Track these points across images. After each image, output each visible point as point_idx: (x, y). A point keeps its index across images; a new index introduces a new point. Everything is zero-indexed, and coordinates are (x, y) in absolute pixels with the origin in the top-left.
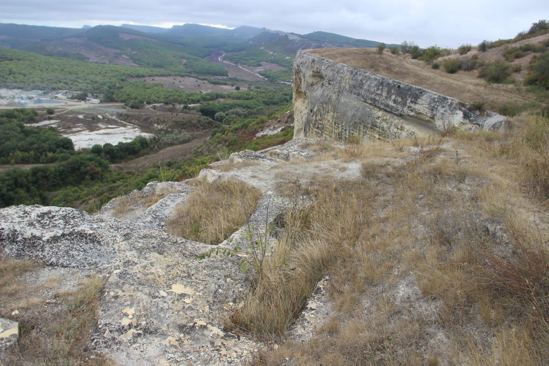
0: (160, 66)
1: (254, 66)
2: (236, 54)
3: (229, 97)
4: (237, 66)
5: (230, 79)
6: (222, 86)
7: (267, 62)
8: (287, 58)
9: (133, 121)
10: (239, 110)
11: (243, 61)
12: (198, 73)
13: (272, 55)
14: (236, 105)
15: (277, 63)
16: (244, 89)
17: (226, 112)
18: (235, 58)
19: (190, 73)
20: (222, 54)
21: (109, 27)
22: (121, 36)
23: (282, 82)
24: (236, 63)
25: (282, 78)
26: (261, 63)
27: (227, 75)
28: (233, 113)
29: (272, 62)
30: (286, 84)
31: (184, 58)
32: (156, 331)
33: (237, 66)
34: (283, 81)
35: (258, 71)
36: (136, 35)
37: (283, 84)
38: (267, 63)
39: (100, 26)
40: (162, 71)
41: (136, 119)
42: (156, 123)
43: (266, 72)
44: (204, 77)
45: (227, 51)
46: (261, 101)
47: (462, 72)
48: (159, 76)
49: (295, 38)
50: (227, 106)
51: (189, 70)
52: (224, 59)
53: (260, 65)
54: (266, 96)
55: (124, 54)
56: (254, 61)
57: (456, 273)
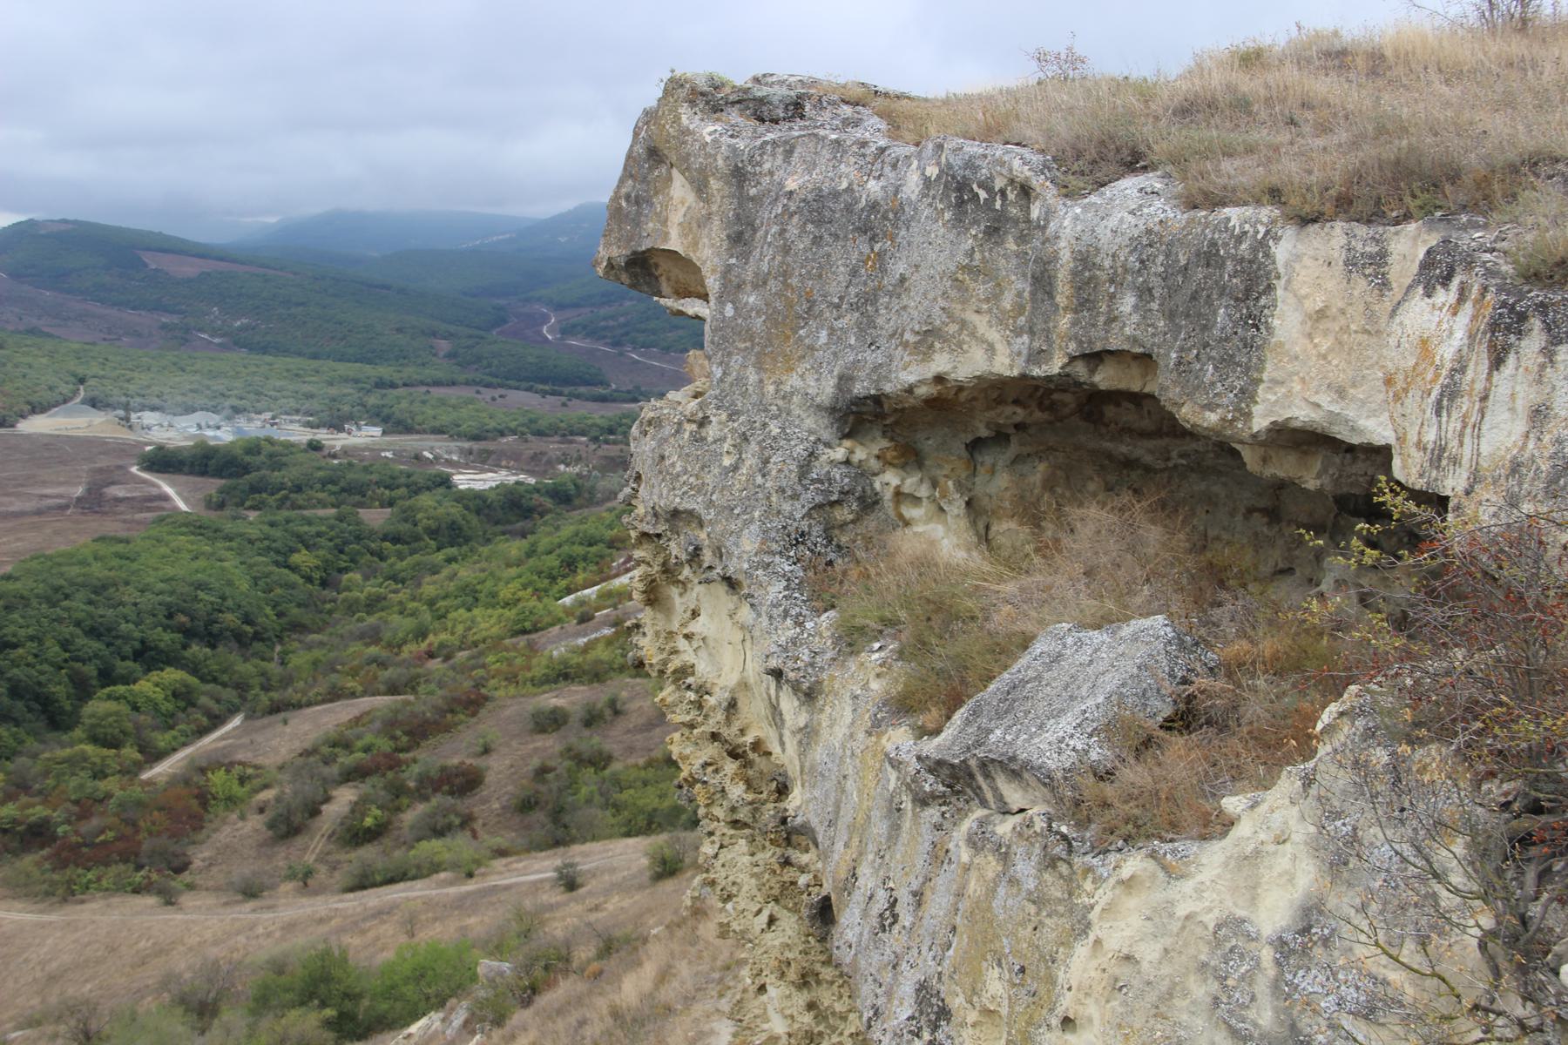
2: (604, 311)
9: (504, 463)
11: (641, 338)
18: (605, 328)
22: (147, 257)
24: (616, 344)
27: (606, 384)
32: (537, 803)
33: (621, 354)
40: (410, 372)
41: (510, 458)
42: (562, 462)
45: (560, 307)
47: (1472, 161)
55: (200, 330)
56: (681, 332)
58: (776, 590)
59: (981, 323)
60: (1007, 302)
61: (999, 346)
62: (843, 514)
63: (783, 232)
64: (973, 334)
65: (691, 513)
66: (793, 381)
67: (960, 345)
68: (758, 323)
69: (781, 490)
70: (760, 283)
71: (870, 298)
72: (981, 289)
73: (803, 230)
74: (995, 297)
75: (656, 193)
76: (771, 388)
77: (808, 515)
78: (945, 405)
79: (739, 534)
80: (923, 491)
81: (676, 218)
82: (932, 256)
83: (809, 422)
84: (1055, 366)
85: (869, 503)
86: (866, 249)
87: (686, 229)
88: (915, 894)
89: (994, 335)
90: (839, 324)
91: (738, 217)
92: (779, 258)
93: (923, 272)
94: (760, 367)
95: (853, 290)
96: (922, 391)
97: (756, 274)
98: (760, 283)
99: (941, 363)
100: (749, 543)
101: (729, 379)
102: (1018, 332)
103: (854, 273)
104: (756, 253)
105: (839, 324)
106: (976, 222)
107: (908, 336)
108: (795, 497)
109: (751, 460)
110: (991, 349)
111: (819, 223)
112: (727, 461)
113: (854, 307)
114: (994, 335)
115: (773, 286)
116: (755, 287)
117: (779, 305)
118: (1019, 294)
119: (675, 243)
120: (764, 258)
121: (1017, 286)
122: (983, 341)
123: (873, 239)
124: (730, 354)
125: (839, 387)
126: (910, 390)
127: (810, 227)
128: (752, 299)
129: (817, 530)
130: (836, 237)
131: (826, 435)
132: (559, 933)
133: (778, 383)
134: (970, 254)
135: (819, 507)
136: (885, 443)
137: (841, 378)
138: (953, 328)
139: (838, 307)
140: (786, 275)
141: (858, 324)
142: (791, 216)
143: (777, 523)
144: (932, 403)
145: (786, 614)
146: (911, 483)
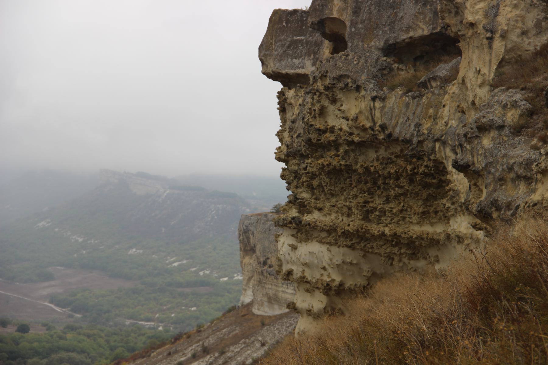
8: (133, 251)
34: (131, 318)
35: (45, 292)
58: (371, 86)
59: (421, 24)
60: (427, 19)
61: (425, 29)
62: (385, 72)
63: (369, 9)
64: (419, 27)
65: (346, 75)
66: (373, 43)
67: (416, 30)
68: (362, 31)
69: (371, 66)
70: (363, 22)
71: (393, 22)
72: (421, 17)
73: (375, 8)
74: (425, 18)
75: (329, 3)
76: (366, 46)
77: (378, 71)
78: (412, 43)
79: (361, 76)
80: (404, 68)
81: (335, 9)
82: (409, 11)
83: (376, 53)
84: (438, 29)
85: (391, 70)
86: (392, 11)
87: (339, 11)
88: (176, 350)
89: (424, 27)
90: (385, 29)
91: (356, 7)
92: (368, 15)
93: (407, 14)
94: (363, 41)
95: (388, 21)
96: (407, 40)
97: (361, 20)
98: (363, 22)
99: (411, 34)
100: (364, 77)
101: (354, 46)
102: (430, 25)
103: (389, 17)
104: (362, 15)
105: (385, 29)
106: (421, 2)
107: (404, 28)
108: (375, 67)
109: (362, 61)
110: (423, 30)
111: (379, 6)
112: (355, 63)
113: (388, 25)
114: (424, 27)
115: (366, 22)
116: (361, 23)
117: (368, 26)
118: (430, 17)
119: (335, 15)
120: (364, 16)
121: (430, 15)
122: (421, 28)
123: (394, 9)
124: (354, 40)
125: (385, 43)
126: (404, 40)
127: (377, 7)
128: (360, 26)
129: (380, 75)
130: (384, 9)
131: (381, 55)
132: (339, 96)
133: (368, 45)
134: (419, 9)
135: (380, 69)
136: (394, 58)
137: (385, 41)
138: (414, 26)
139: (385, 25)
140: (370, 19)
141: (390, 29)
142: (372, 5)
143: (370, 73)
144: (408, 43)
145: (374, 90)
146: (401, 66)
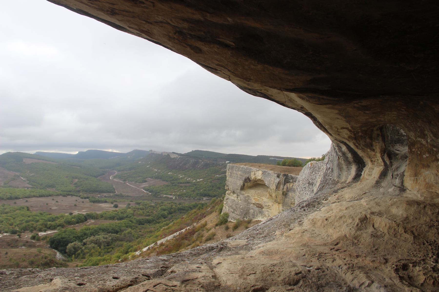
0: (52, 186)
1: (140, 182)
3: (102, 216)
4: (125, 183)
5: (117, 195)
6: (101, 204)
7: (152, 178)
8: (169, 173)
10: (101, 237)
12: (86, 191)
13: (156, 172)
14: (100, 229)
15: (161, 179)
16: (122, 206)
17: (84, 241)
19: (79, 191)
20: (115, 173)
21: (64, 154)
23: (164, 196)
24: (125, 180)
25: (164, 192)
26: (147, 179)
28: (92, 242)
29: (157, 178)
30: (168, 198)
31: (76, 178)
34: (165, 194)
35: (143, 186)
36: (43, 160)
37: (165, 197)
38: (152, 179)
39: (198, 151)
43: (150, 187)
44: (85, 196)
46: (134, 221)
48: (37, 197)
49: (175, 156)
50: (87, 232)
51: (78, 189)
52: (115, 177)
53: (146, 181)
54: (143, 213)
55: (22, 177)
57: (347, 196)
